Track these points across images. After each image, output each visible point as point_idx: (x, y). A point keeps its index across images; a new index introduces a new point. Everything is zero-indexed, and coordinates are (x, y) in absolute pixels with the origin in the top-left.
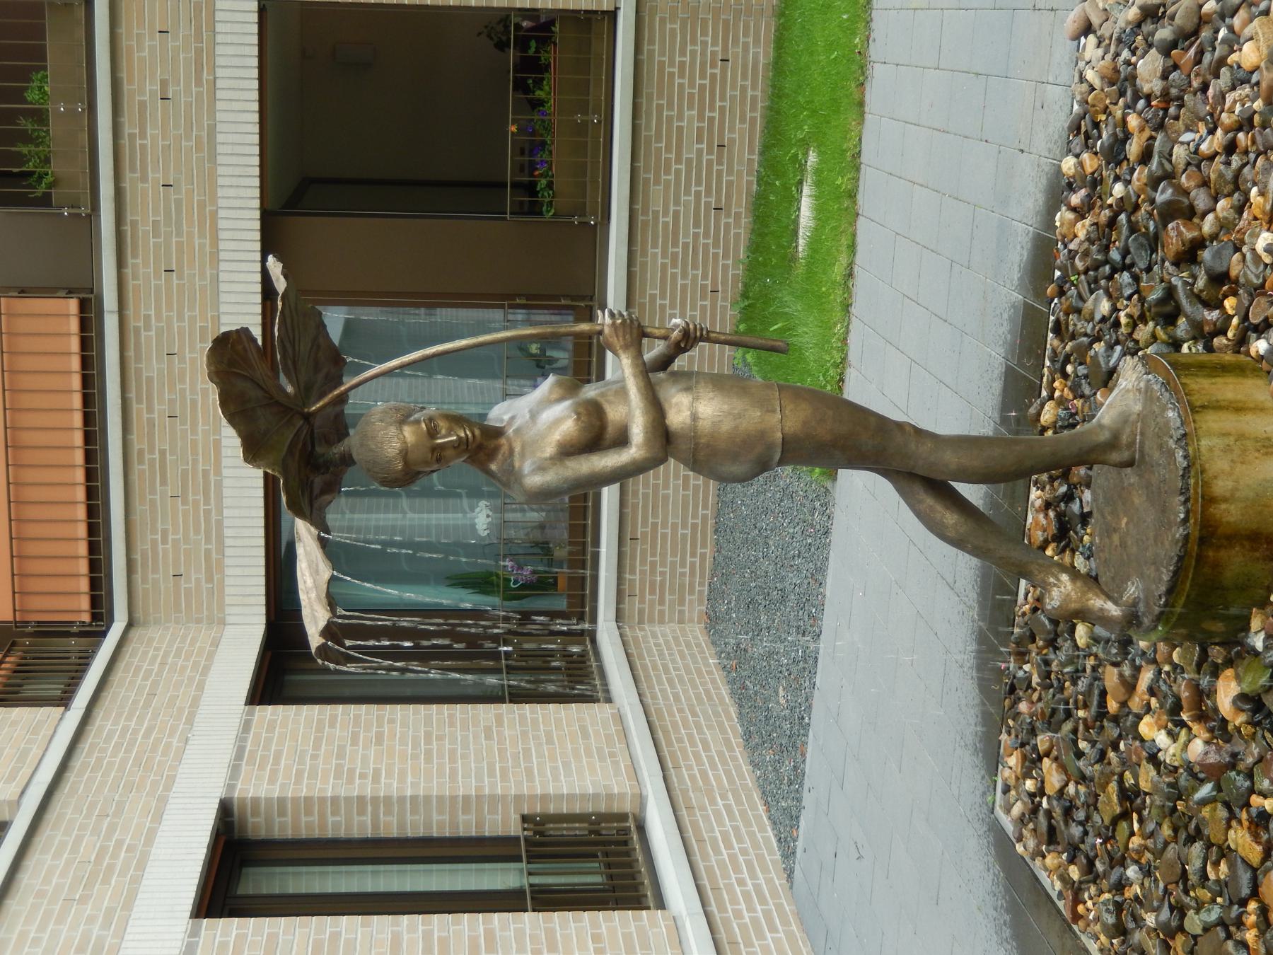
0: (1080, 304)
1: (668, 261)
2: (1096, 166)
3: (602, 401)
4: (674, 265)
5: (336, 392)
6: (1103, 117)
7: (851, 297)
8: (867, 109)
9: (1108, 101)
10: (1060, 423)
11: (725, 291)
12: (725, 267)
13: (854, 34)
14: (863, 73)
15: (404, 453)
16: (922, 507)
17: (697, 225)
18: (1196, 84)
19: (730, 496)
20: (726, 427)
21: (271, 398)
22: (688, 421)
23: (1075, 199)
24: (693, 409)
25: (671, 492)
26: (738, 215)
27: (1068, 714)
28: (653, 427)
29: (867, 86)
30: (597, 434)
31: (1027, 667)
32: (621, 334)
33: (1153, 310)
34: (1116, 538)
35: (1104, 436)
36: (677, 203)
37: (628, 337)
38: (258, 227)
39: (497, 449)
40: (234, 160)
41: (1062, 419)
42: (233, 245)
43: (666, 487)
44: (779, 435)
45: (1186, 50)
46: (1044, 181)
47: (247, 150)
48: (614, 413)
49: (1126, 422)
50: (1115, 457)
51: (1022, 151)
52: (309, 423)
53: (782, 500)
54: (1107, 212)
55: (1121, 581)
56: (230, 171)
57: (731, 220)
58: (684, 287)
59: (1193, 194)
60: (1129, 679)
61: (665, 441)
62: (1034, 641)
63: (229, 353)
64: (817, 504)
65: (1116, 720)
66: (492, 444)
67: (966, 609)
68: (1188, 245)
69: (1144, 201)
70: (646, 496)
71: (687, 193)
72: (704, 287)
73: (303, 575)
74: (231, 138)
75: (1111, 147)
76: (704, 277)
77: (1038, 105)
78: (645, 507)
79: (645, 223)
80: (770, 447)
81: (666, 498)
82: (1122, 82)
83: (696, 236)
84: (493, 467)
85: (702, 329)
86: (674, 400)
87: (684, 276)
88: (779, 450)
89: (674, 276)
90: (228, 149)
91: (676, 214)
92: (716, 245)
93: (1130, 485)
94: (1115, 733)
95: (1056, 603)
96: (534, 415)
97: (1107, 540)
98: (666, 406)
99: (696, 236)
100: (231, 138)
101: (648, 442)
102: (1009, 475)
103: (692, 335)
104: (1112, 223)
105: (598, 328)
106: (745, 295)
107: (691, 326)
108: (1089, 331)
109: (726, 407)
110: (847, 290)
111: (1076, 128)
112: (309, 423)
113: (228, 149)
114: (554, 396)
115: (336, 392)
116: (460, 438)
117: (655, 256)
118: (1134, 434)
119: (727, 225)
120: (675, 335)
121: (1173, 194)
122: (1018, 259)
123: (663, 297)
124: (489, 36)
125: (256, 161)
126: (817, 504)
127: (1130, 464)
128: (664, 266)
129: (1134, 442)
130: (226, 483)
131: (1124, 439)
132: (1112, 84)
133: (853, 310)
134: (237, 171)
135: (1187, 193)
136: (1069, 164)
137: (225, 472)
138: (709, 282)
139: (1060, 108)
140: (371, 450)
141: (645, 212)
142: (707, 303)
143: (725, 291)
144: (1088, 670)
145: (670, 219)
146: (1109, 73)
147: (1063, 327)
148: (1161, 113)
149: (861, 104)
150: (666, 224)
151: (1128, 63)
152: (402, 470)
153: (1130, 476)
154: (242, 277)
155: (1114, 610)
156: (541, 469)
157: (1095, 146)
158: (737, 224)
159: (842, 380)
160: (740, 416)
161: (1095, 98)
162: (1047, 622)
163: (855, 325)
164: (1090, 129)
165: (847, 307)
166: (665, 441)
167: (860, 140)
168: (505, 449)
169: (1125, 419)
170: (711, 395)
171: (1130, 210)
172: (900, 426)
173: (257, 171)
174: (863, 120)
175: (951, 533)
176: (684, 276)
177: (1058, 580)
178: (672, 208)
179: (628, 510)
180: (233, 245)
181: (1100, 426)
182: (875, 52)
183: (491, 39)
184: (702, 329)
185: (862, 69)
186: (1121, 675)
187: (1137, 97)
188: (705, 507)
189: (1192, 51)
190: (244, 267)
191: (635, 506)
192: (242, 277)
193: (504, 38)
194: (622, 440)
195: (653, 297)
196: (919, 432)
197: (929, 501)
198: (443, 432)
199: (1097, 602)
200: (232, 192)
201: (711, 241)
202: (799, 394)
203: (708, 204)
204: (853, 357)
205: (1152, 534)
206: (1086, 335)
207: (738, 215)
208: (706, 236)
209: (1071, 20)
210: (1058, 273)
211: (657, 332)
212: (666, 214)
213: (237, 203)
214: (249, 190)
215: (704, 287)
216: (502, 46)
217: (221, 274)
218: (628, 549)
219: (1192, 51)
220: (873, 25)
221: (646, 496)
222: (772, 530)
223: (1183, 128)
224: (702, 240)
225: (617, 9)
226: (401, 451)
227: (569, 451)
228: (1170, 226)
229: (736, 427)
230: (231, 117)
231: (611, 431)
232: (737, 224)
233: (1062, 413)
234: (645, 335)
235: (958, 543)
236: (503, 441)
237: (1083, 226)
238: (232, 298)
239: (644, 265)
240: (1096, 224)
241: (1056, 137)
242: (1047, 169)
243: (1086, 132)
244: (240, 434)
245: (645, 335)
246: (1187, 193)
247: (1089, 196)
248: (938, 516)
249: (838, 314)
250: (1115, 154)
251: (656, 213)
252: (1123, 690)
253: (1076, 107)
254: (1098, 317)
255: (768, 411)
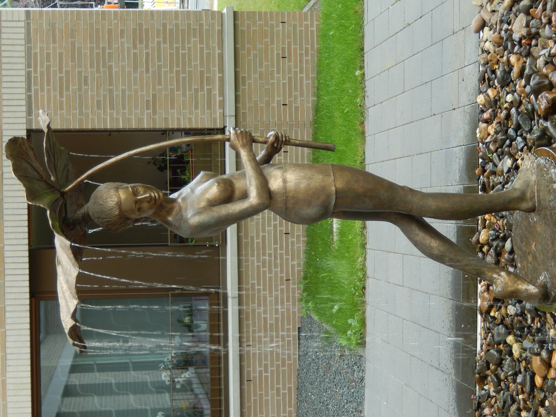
0: (495, 169)
1: (261, 264)
2: (496, 94)
3: (232, 179)
4: (264, 266)
5: (79, 180)
6: (497, 67)
7: (365, 238)
8: (366, 135)
9: (498, 57)
10: (491, 238)
11: (293, 279)
12: (293, 266)
13: (356, 97)
14: (363, 116)
15: (119, 204)
16: (418, 238)
17: (275, 243)
18: (544, 21)
19: (304, 395)
20: (303, 185)
21: (42, 178)
22: (281, 184)
23: (486, 116)
24: (285, 178)
25: (270, 398)
26: (298, 236)
27: (514, 401)
28: (262, 186)
29: (366, 123)
30: (229, 195)
31: (486, 387)
32: (240, 138)
33: (536, 143)
34: (530, 258)
35: (516, 194)
36: (264, 231)
37: (244, 140)
38: (28, 285)
39: (172, 209)
40: (13, 218)
41: (492, 236)
42: (13, 266)
43: (267, 395)
44: (334, 188)
45: (536, 8)
46: (468, 118)
47: (21, 212)
48: (239, 185)
49: (528, 186)
50: (525, 205)
51: (454, 109)
52: (63, 198)
53: (335, 378)
54: (504, 112)
55: (536, 273)
56: (11, 224)
57: (295, 240)
58: (270, 278)
59: (550, 76)
60: (546, 360)
61: (269, 199)
62: (489, 368)
63: (14, 142)
64: (355, 367)
65: (542, 389)
66: (170, 206)
67: (447, 376)
68: (551, 103)
69: (524, 98)
70: (255, 401)
71: (269, 225)
72: (282, 278)
73: (61, 284)
74: (12, 205)
75: (503, 78)
76: (282, 272)
77: (461, 80)
78: (255, 408)
79: (247, 243)
80: (329, 196)
81: (267, 401)
82: (504, 43)
83: (275, 249)
84: (170, 219)
85: (286, 137)
86: (273, 174)
87: (270, 272)
88: (334, 197)
89: (264, 272)
90: (10, 212)
91: (264, 237)
92: (287, 254)
93: (535, 222)
94: (542, 395)
95: (499, 289)
96: (193, 190)
97: (525, 262)
98: (268, 178)
99: (275, 249)
100: (12, 205)
101: (259, 194)
102: (464, 211)
103: (280, 139)
104: (508, 117)
105: (228, 137)
106: (305, 278)
107: (280, 135)
108: (501, 180)
109: (302, 174)
110: (363, 235)
111: (482, 80)
112: (63, 198)
113: (10, 212)
114: (204, 180)
115: (79, 180)
116: (151, 196)
117: (253, 261)
118: (533, 192)
119: (293, 243)
120: (271, 139)
121: (539, 79)
122: (458, 166)
123: (259, 284)
124: (154, 163)
125: (26, 217)
126: (355, 367)
127: (532, 210)
128: (258, 267)
129: (534, 197)
130: (9, 405)
131: (528, 195)
132: (499, 46)
133: (368, 246)
134: (16, 224)
135: (546, 76)
136: (481, 99)
137: (9, 399)
138: (284, 275)
139: (472, 74)
140: (100, 205)
141: (246, 237)
142: (284, 287)
143: (293, 279)
144: (522, 370)
145: (260, 240)
146: (498, 40)
147: (487, 185)
148: (528, 47)
149: (363, 133)
150: (258, 243)
151: (506, 31)
152: (119, 215)
153: (534, 218)
154: (18, 284)
155: (533, 289)
156: (199, 213)
157: (494, 84)
158: (298, 242)
159: (364, 288)
160: (310, 178)
161: (491, 56)
162: (495, 353)
163: (370, 254)
164: (490, 75)
165: (364, 246)
166: (269, 199)
167: (364, 153)
168: (176, 209)
169: (527, 184)
170: (293, 169)
171: (517, 105)
172: (403, 188)
173: (26, 223)
174: (365, 141)
175: (436, 252)
176: (270, 272)
177: (500, 275)
178: (261, 234)
179: (246, 410)
180: (13, 266)
181: (514, 189)
182: (368, 102)
183: (156, 165)
184: (286, 137)
185: (362, 114)
186: (542, 360)
187: (513, 46)
188: (290, 406)
189: (540, 7)
190: (19, 278)
191: (249, 407)
192: (18, 284)
193: (163, 165)
194: (245, 196)
195: (253, 285)
196: (412, 190)
197: (421, 235)
198: (142, 192)
199: (523, 286)
200: (12, 236)
201: (284, 252)
202: (342, 168)
203: (281, 231)
204: (369, 272)
205: (550, 243)
206: (500, 183)
207: (298, 236)
208: (281, 248)
209: (474, 23)
210: (481, 160)
211: (261, 139)
212: (258, 238)
213: (15, 242)
214: (22, 234)
215: (282, 278)
216: (162, 169)
217: (6, 283)
218: (245, 387)
219: (540, 7)
220: (366, 89)
221: (255, 401)
222: (330, 399)
223: (541, 49)
224: (279, 251)
225: (225, 127)
226: (117, 203)
227: (213, 204)
228: (540, 97)
229: (309, 184)
230: (12, 194)
231: (237, 193)
232: (298, 242)
233: (492, 232)
234: (254, 141)
235: (439, 258)
236: (176, 204)
237: (492, 127)
238: (13, 296)
239: (247, 267)
240: (500, 123)
241: (472, 91)
242: (468, 111)
243: (488, 78)
244: (25, 186)
245: (254, 141)
246: (546, 76)
247: (493, 111)
248: (428, 242)
249: (359, 250)
250: (506, 82)
251: (252, 238)
252: (544, 368)
253: (481, 69)
254: (505, 170)
255: (326, 175)
